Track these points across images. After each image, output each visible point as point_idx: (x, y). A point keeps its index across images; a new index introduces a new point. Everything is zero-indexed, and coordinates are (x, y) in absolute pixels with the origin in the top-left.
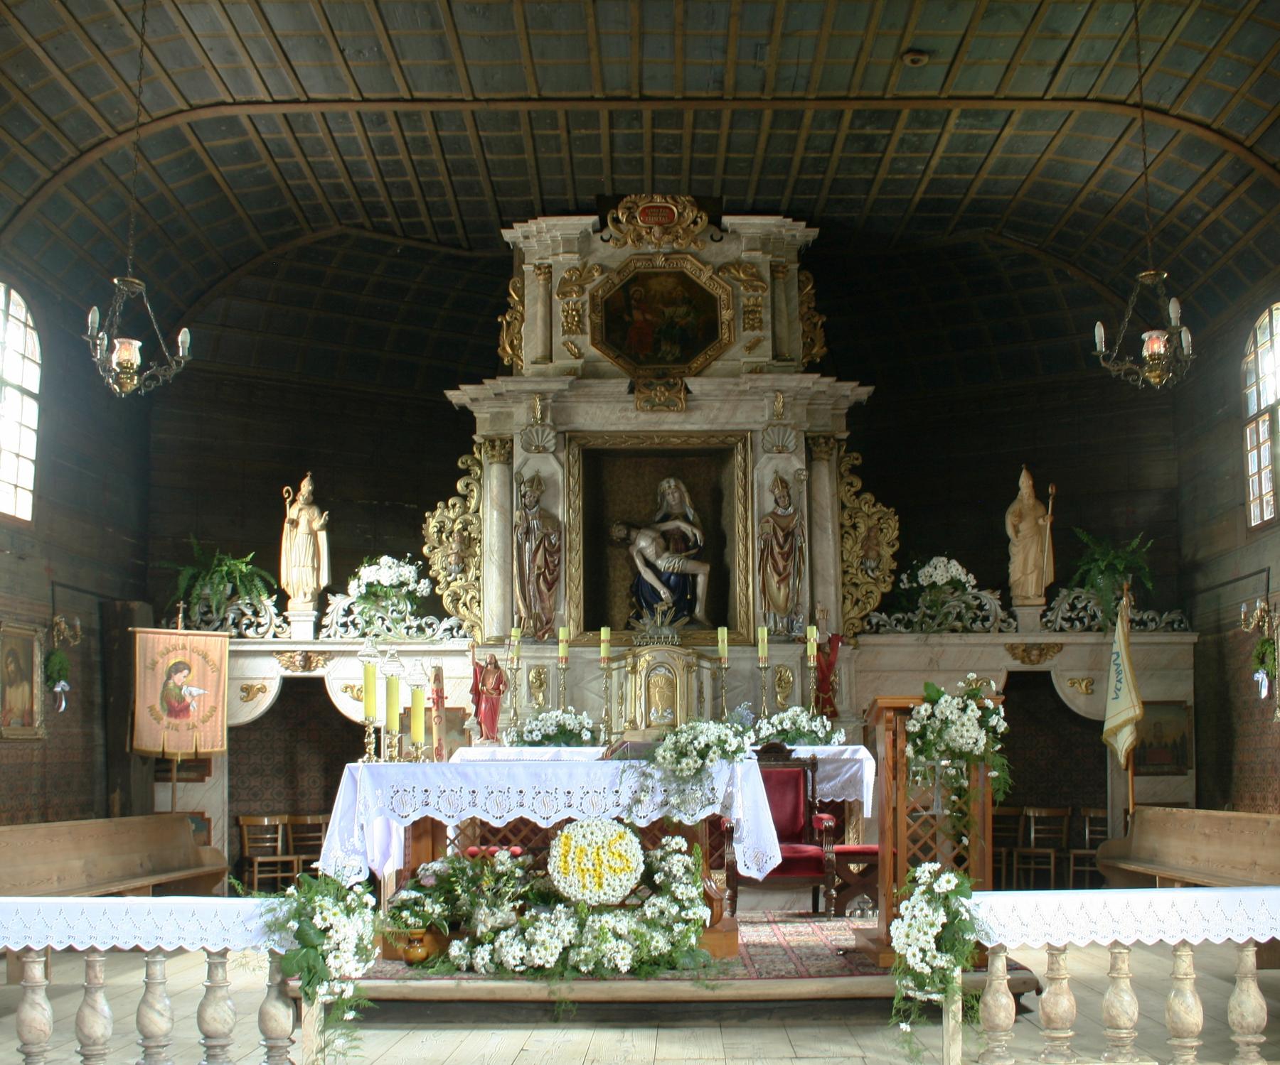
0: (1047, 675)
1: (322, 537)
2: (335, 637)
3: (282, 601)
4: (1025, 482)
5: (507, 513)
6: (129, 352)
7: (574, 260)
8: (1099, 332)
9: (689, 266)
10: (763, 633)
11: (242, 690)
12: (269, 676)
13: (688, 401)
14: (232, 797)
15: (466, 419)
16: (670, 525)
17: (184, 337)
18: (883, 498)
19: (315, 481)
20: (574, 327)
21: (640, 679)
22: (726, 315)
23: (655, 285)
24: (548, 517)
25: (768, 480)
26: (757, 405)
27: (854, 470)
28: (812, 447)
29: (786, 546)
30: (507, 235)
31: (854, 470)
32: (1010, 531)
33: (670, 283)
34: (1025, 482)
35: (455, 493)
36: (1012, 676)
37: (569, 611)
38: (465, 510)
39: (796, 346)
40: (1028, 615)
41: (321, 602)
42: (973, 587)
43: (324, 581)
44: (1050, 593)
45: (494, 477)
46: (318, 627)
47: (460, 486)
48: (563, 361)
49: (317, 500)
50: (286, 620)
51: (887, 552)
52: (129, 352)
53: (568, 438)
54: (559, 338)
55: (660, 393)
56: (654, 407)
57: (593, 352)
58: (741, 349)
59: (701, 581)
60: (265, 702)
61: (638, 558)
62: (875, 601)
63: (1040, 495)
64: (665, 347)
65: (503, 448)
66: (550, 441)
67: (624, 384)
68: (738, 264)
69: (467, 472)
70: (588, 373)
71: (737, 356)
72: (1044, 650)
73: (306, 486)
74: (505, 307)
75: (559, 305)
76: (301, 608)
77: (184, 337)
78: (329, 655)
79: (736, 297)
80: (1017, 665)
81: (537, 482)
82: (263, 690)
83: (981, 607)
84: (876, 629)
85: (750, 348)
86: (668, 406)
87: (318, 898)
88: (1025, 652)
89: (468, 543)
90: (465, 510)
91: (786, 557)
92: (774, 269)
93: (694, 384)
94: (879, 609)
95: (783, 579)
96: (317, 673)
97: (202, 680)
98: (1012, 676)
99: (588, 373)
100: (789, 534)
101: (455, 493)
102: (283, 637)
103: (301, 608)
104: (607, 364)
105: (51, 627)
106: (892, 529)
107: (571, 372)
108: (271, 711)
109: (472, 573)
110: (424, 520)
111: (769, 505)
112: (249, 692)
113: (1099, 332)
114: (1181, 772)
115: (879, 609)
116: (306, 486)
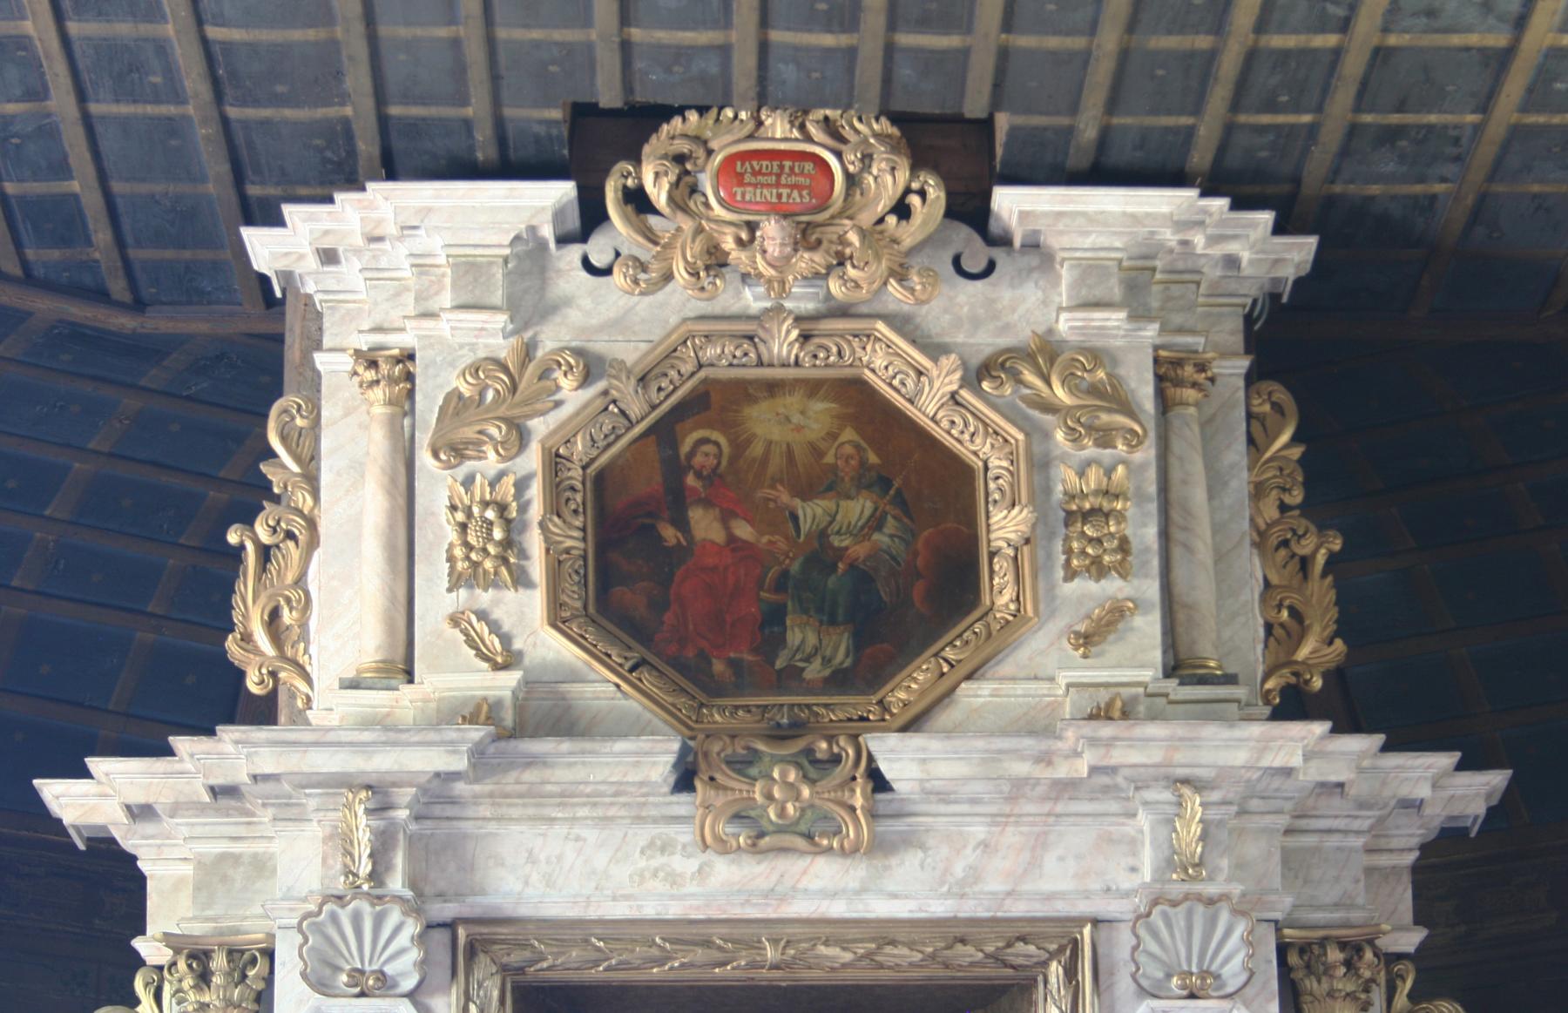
9: (882, 362)
22: (1005, 525)
23: (767, 424)
33: (818, 416)
56: (760, 836)
57: (551, 647)
64: (799, 634)
67: (656, 757)
68: (1045, 353)
79: (1041, 464)
85: (1087, 640)
86: (810, 834)
92: (1169, 373)
104: (600, 688)
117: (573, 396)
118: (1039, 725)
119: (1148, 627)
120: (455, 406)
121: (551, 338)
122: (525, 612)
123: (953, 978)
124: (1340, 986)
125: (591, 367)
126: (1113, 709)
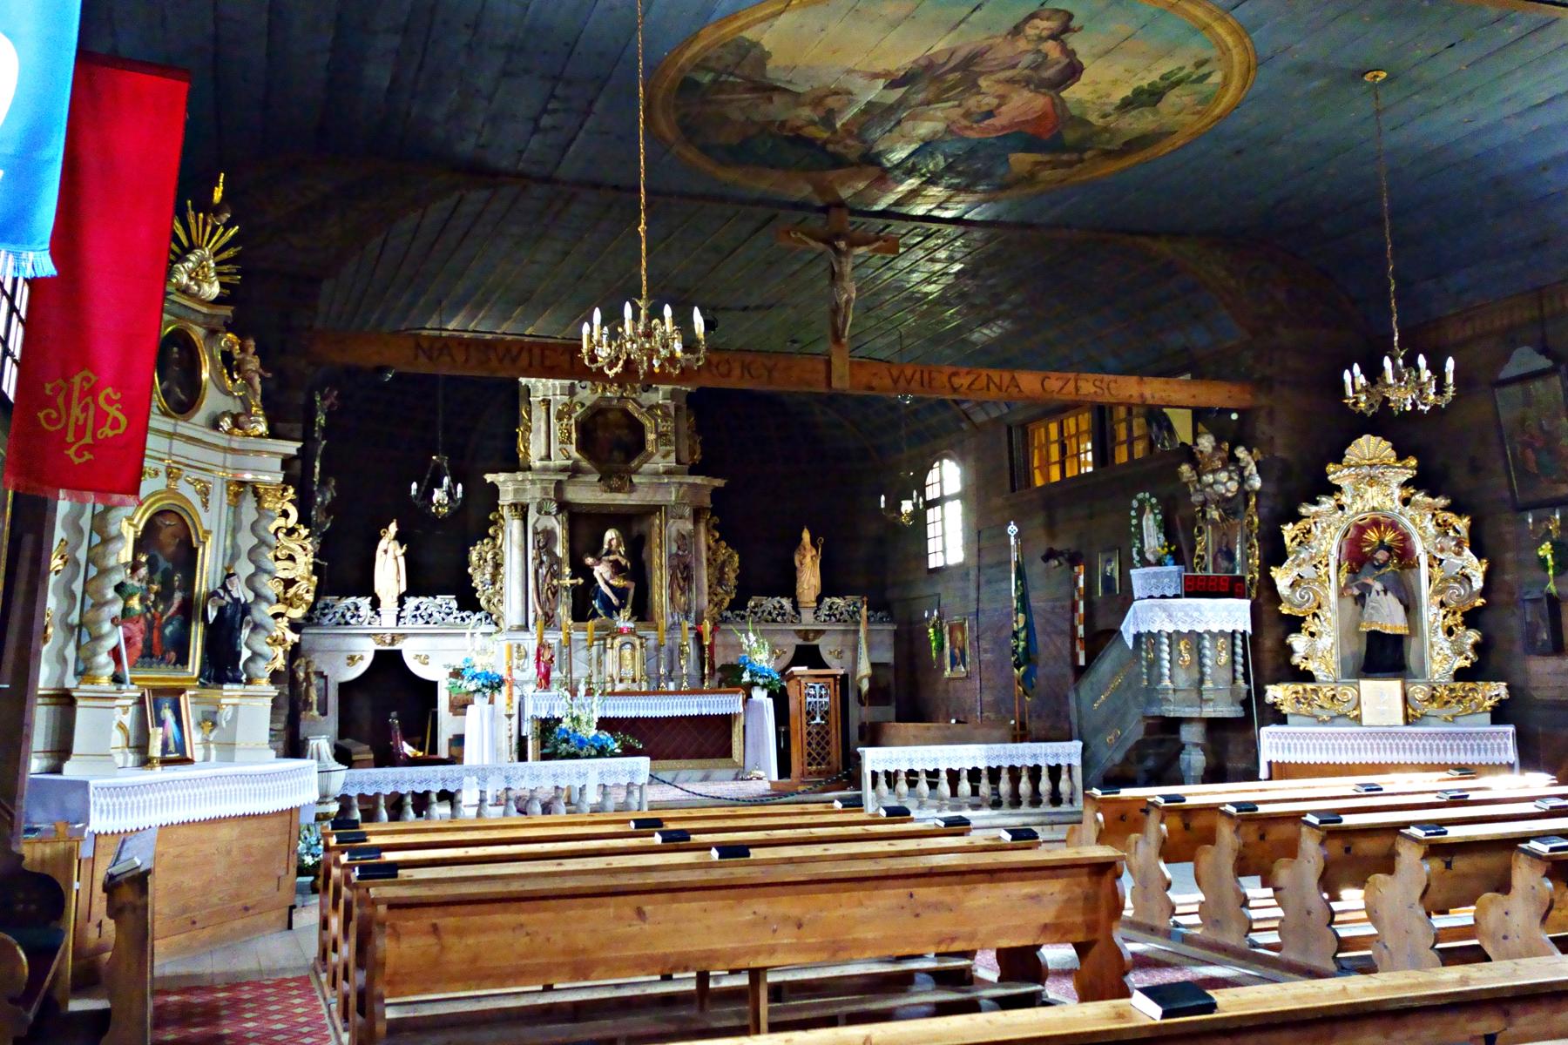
0: (399, 652)
1: (402, 561)
2: (408, 625)
3: (375, 604)
4: (806, 536)
7: (566, 399)
8: (414, 486)
9: (630, 407)
11: (427, 657)
12: (366, 650)
13: (633, 488)
16: (612, 557)
19: (398, 525)
20: (566, 440)
21: (616, 652)
22: (651, 437)
23: (611, 416)
25: (674, 534)
26: (660, 479)
28: (697, 515)
29: (683, 574)
30: (523, 380)
31: (716, 527)
32: (797, 563)
33: (619, 415)
34: (806, 536)
35: (488, 536)
36: (377, 652)
37: (563, 611)
38: (494, 546)
40: (807, 616)
41: (401, 601)
43: (403, 588)
44: (819, 600)
45: (513, 526)
46: (399, 618)
47: (491, 531)
48: (558, 461)
50: (378, 614)
53: (563, 506)
55: (615, 482)
56: (612, 490)
57: (576, 455)
59: (632, 592)
61: (599, 577)
62: (726, 604)
63: (814, 543)
64: (616, 454)
66: (553, 507)
67: (596, 478)
68: (658, 406)
69: (495, 523)
70: (574, 471)
72: (819, 633)
78: (404, 636)
79: (657, 425)
80: (800, 642)
82: (361, 658)
83: (782, 607)
85: (664, 457)
86: (619, 490)
88: (804, 634)
90: (494, 546)
91: (684, 579)
92: (677, 409)
94: (729, 608)
95: (683, 593)
96: (396, 647)
98: (377, 652)
101: (488, 536)
102: (376, 624)
104: (584, 464)
107: (563, 469)
109: (498, 586)
110: (468, 552)
111: (674, 549)
113: (414, 486)
114: (888, 704)
117: (579, 410)
118: (656, 474)
119: (673, 457)
120: (560, 412)
121: (576, 399)
122: (572, 449)
123: (1420, 985)
124: (948, 351)
125: (583, 405)
126: (669, 472)
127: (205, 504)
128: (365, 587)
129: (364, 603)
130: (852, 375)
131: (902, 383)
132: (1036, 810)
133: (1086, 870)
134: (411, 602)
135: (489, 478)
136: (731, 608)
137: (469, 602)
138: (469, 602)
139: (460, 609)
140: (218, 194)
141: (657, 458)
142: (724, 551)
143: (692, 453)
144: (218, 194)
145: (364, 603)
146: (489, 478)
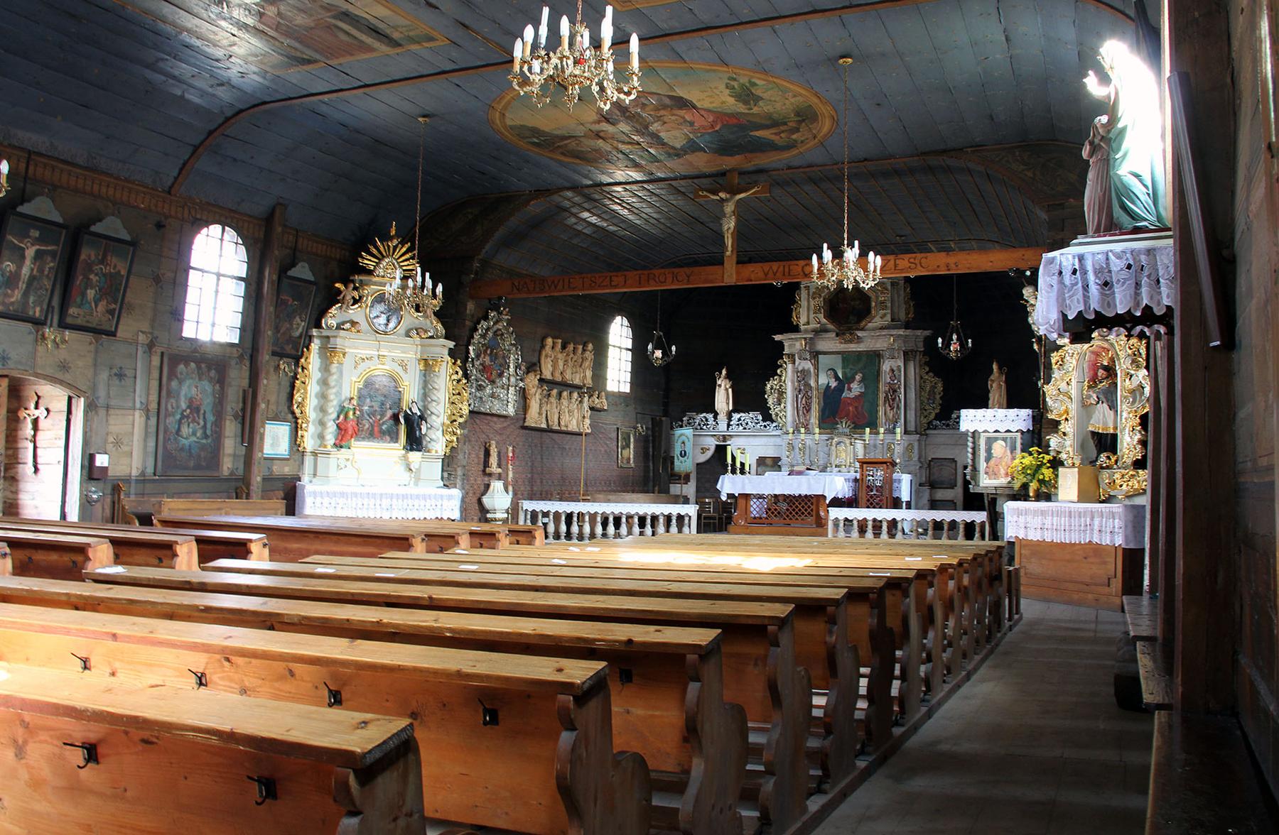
2: (735, 429)
3: (716, 415)
4: (995, 366)
5: (793, 382)
6: (658, 354)
8: (940, 340)
10: (882, 430)
13: (859, 340)
14: (697, 491)
15: (780, 345)
17: (674, 348)
18: (937, 375)
24: (807, 385)
27: (926, 363)
28: (907, 356)
31: (926, 363)
34: (995, 366)
39: (902, 316)
41: (730, 418)
42: (875, 432)
46: (729, 425)
48: (813, 325)
49: (728, 377)
51: (938, 397)
52: (658, 354)
54: (812, 316)
58: (879, 319)
60: (709, 454)
62: (932, 416)
65: (792, 357)
71: (877, 321)
73: (724, 372)
74: (794, 302)
75: (812, 303)
76: (722, 418)
77: (674, 348)
81: (803, 371)
84: (936, 428)
86: (851, 342)
87: (298, 319)
89: (781, 394)
93: (860, 334)
94: (936, 419)
95: (892, 409)
97: (691, 445)
99: (824, 330)
100: (895, 391)
103: (722, 418)
104: (830, 326)
105: (635, 428)
106: (940, 387)
108: (713, 456)
112: (704, 450)
113: (940, 340)
115: (936, 419)
116: (724, 372)
127: (406, 370)
128: (710, 408)
129: (710, 416)
130: (738, 273)
131: (771, 274)
132: (939, 542)
133: (241, 472)
134: (736, 416)
135: (777, 338)
136: (938, 417)
137: (767, 417)
138: (767, 417)
139: (764, 420)
140: (393, 233)
141: (877, 319)
142: (931, 379)
143: (907, 314)
144: (393, 233)
145: (710, 416)
146: (777, 338)
